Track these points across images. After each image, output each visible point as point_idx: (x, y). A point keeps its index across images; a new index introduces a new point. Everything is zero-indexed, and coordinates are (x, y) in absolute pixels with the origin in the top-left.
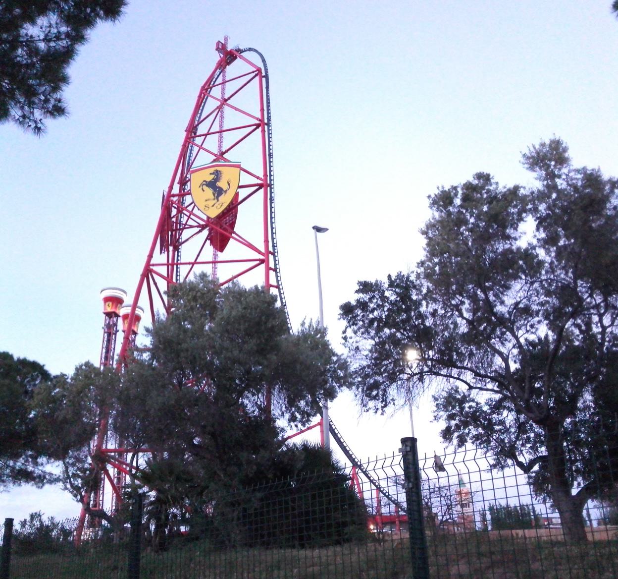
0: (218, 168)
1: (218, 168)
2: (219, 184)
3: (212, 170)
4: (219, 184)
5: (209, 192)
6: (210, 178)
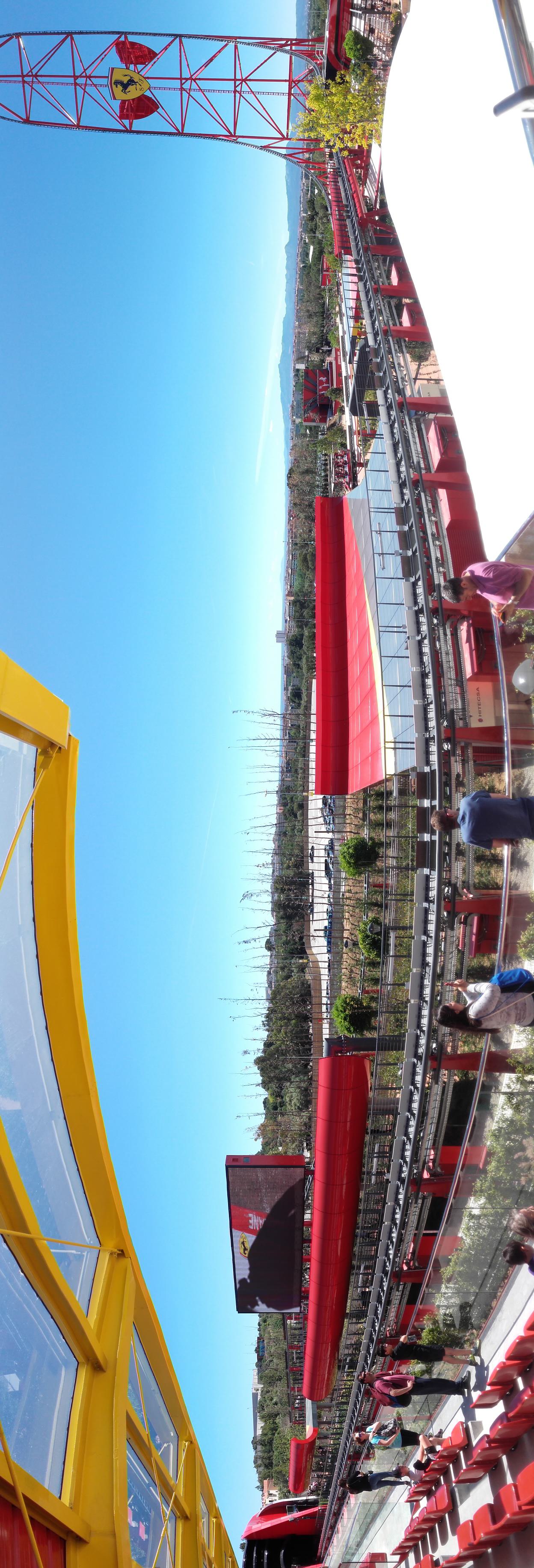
0: (113, 82)
1: (113, 82)
2: (125, 82)
3: (114, 86)
4: (125, 82)
5: (130, 88)
6: (120, 87)
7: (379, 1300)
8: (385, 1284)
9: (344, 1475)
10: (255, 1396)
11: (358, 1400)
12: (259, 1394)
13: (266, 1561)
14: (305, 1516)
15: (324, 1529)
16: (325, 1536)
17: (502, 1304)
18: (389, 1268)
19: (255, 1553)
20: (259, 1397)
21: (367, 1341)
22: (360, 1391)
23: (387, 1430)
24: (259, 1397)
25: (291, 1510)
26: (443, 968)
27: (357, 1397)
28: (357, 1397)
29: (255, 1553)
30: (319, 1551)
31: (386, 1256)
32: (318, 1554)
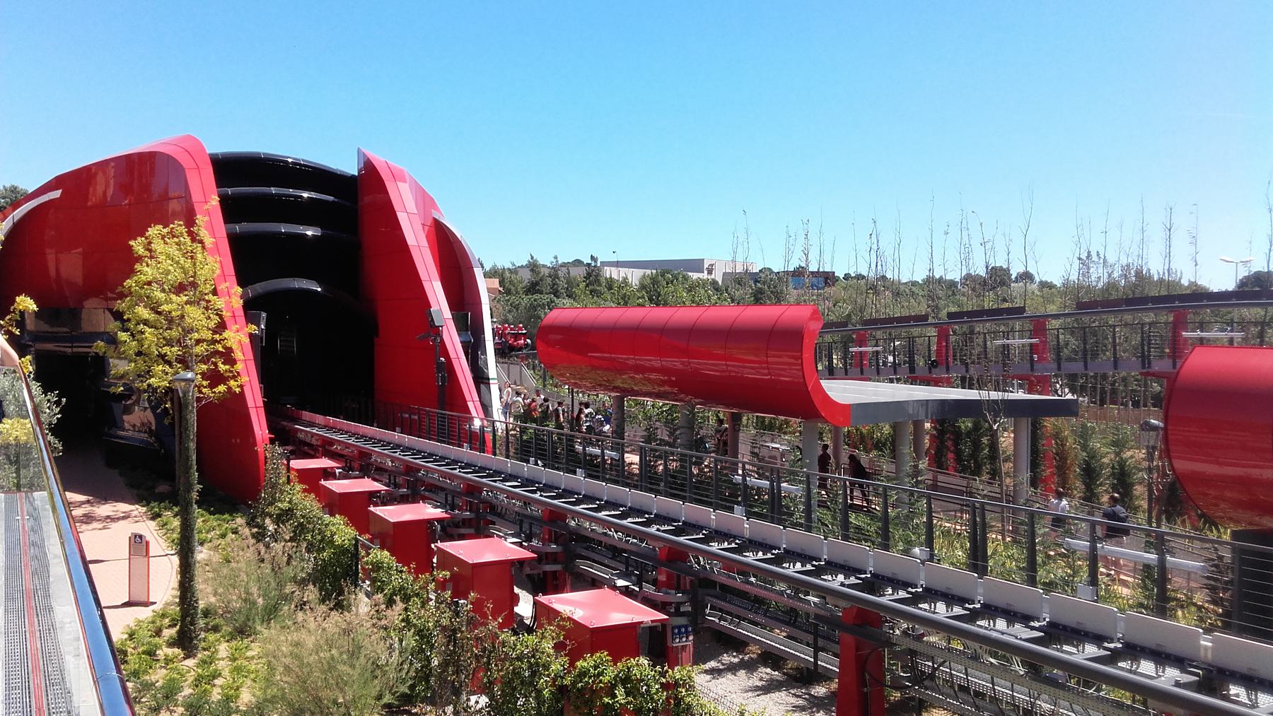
7: (1058, 632)
8: (836, 581)
9: (584, 518)
10: (697, 265)
11: (648, 523)
12: (700, 275)
13: (284, 228)
14: (449, 368)
15: (407, 439)
16: (417, 452)
17: (1266, 677)
18: (888, 597)
19: (313, 195)
20: (695, 276)
21: (526, 475)
22: (677, 532)
23: (398, 694)
24: (695, 276)
25: (461, 325)
26: (1052, 682)
27: (661, 519)
28: (661, 519)
29: (313, 195)
30: (319, 419)
31: (985, 606)
32: (306, 415)
